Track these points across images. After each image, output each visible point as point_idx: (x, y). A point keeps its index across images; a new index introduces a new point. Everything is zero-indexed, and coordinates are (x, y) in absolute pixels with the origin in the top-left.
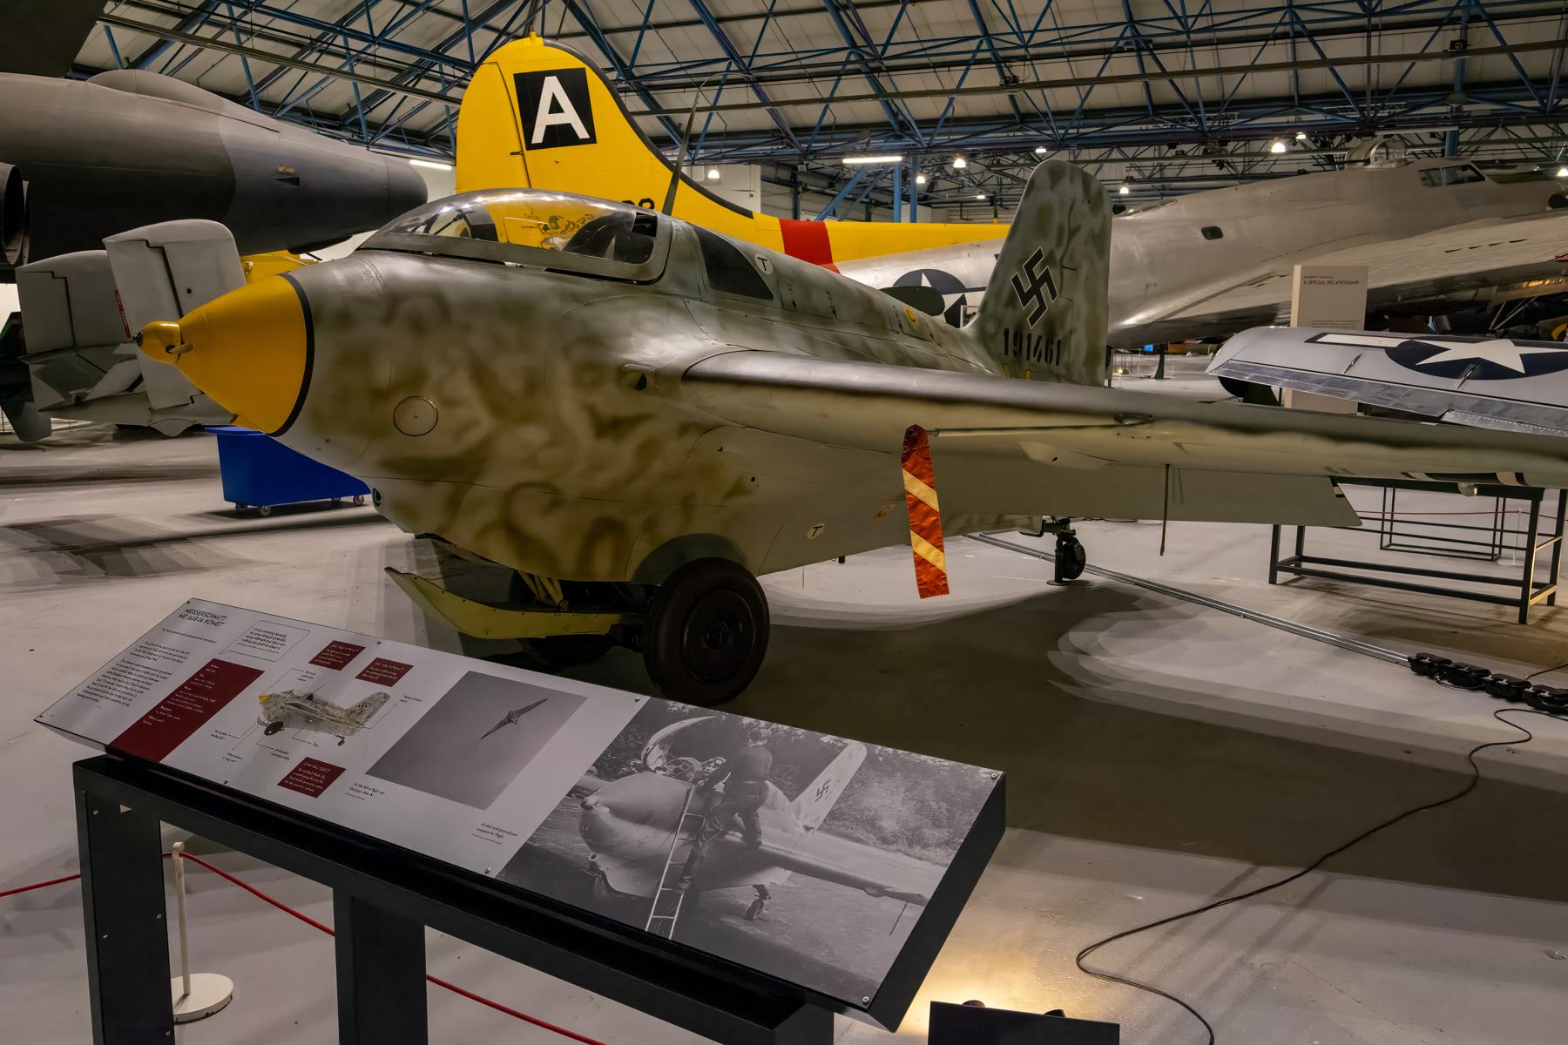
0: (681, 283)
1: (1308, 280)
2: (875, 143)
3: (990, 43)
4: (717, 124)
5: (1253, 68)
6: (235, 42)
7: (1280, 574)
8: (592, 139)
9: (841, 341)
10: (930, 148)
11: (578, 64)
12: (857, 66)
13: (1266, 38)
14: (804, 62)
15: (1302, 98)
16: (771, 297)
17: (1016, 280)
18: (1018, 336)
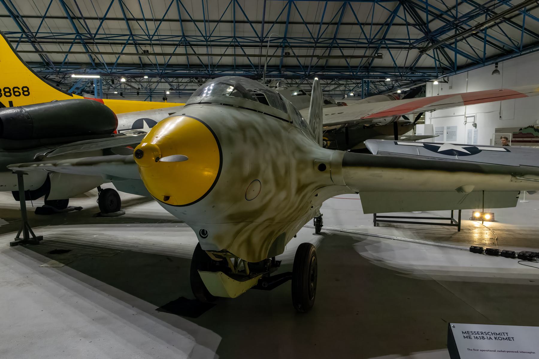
2: (88, 70)
12: (27, 40)
13: (228, 46)
14: (56, 37)
15: (237, 66)
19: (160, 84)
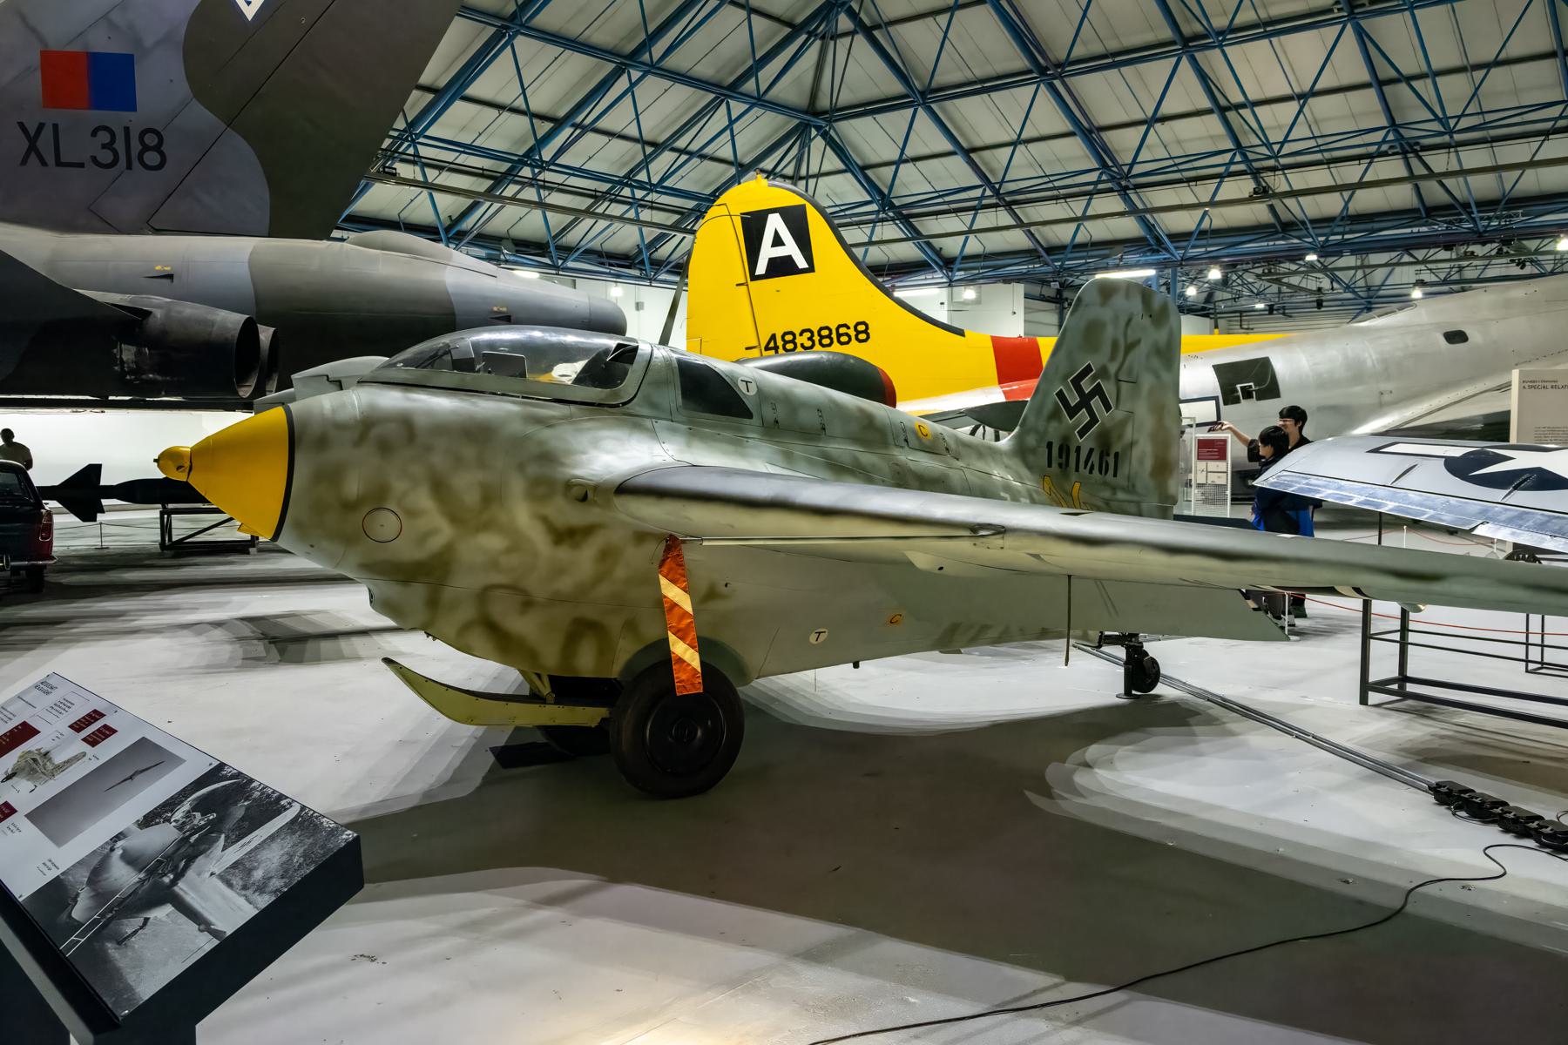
0: (653, 406)
1: (1528, 384)
3: (1244, 155)
4: (974, 246)
5: (1532, 164)
6: (536, 199)
7: (1371, 694)
8: (811, 269)
9: (826, 456)
10: (1185, 260)
11: (803, 202)
12: (1109, 185)
16: (750, 416)
17: (1060, 394)
18: (1064, 449)
19: (1398, 269)
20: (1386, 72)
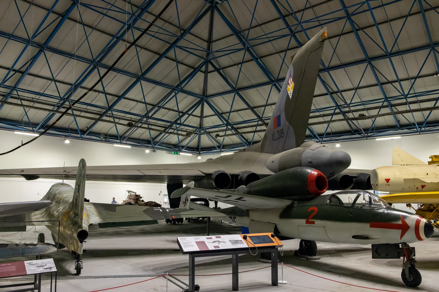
20: (383, 80)
